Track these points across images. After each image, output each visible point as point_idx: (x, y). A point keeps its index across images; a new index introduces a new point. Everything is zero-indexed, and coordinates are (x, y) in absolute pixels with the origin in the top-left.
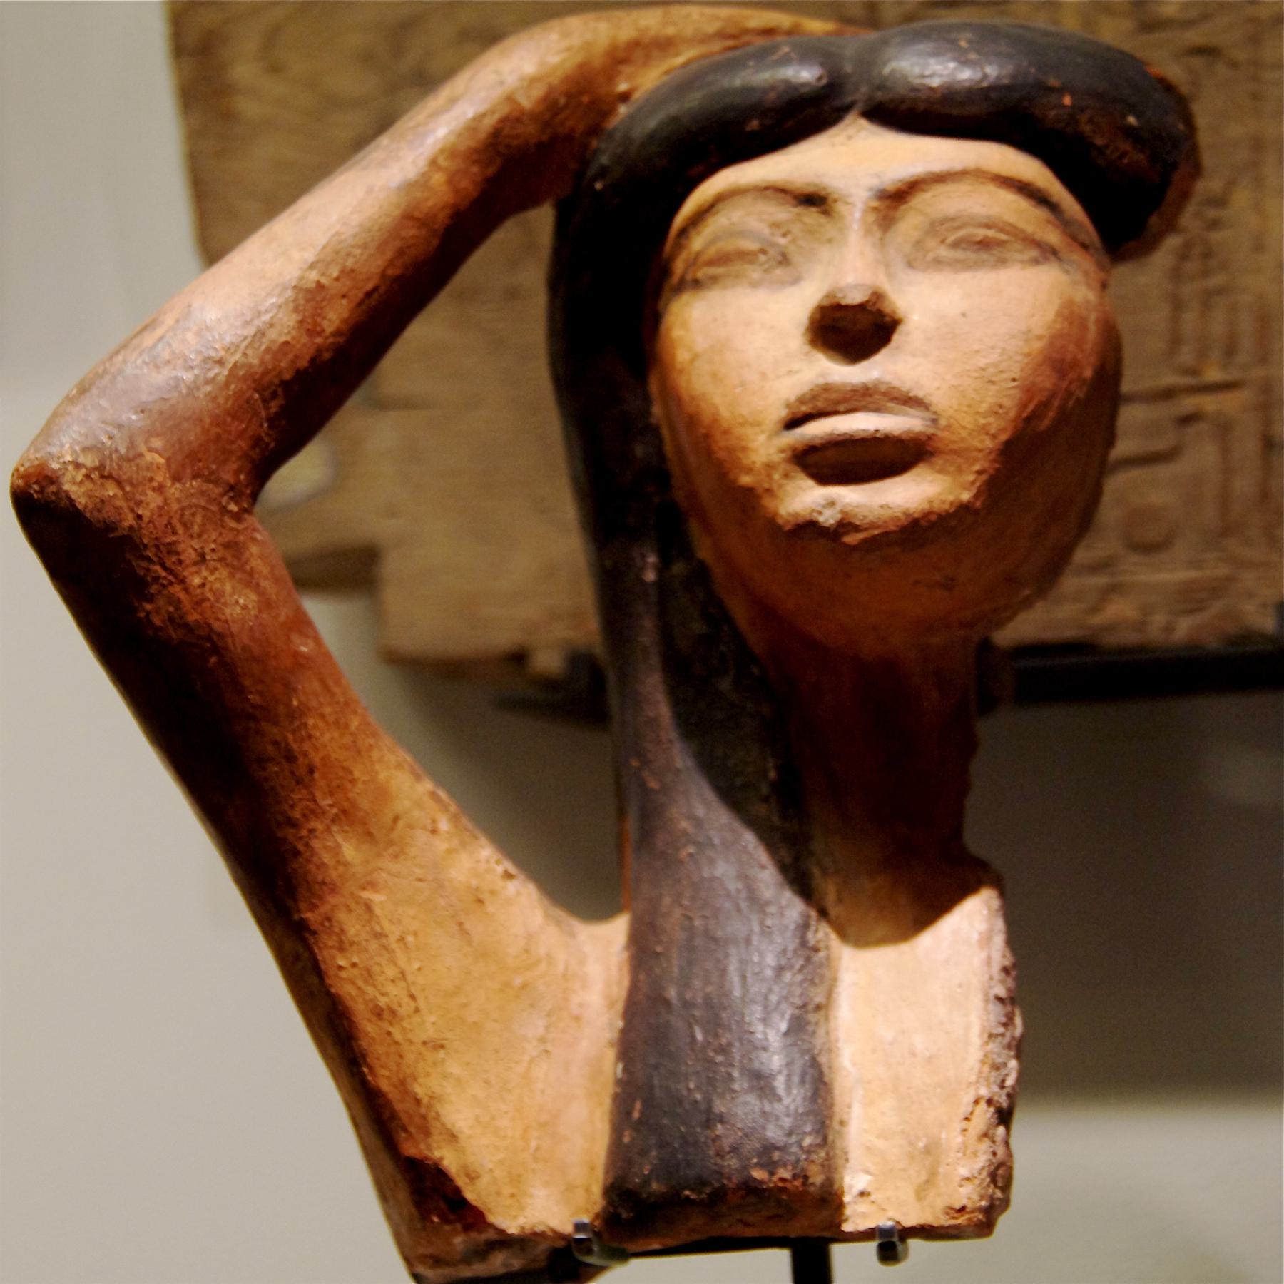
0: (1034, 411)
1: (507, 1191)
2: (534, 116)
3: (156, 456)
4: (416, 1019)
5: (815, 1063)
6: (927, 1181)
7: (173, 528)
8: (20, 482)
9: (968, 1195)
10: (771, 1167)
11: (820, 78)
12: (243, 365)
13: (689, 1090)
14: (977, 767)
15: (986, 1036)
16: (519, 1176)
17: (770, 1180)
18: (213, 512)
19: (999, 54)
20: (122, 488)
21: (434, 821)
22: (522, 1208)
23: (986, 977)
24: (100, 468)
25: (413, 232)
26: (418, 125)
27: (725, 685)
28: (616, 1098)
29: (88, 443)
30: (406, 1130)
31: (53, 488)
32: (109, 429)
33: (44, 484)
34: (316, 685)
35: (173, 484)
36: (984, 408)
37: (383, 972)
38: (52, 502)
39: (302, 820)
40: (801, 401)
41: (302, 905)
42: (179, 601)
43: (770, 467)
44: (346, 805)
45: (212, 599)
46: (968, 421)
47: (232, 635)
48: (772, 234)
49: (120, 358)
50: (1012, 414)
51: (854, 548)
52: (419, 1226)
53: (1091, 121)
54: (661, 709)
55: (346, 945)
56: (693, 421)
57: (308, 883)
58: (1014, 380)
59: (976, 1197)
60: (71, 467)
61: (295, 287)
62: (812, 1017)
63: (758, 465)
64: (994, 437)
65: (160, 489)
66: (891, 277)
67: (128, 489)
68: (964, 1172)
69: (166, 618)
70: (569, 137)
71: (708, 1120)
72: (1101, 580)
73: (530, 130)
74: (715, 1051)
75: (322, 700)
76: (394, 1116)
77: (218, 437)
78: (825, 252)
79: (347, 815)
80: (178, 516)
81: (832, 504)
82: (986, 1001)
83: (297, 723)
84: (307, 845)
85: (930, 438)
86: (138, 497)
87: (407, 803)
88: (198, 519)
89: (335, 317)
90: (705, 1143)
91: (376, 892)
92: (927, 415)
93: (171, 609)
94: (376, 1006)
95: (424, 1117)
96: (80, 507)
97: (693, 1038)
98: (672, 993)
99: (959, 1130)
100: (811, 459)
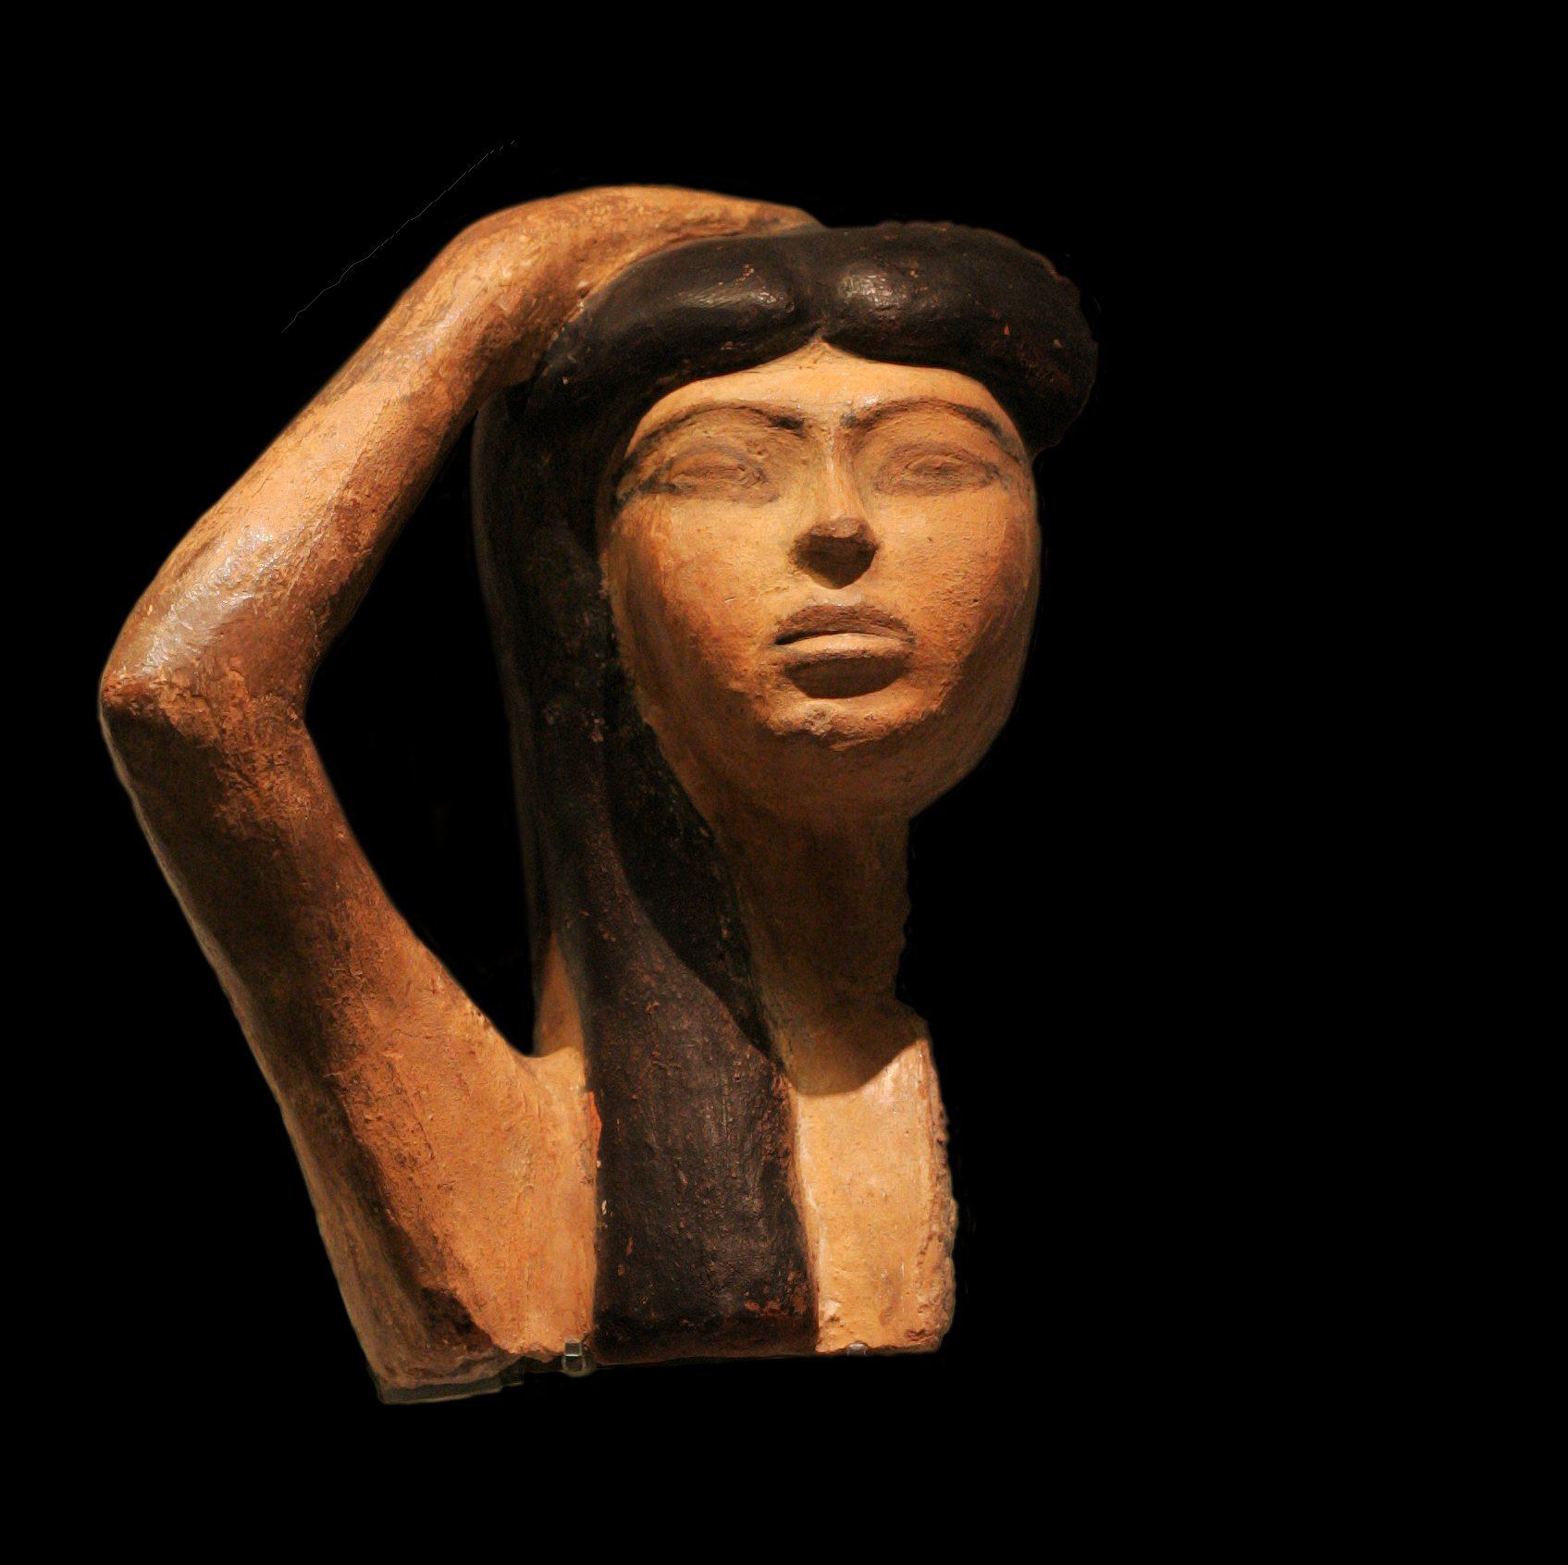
0: (990, 628)
1: (509, 1316)
2: (511, 320)
3: (237, 674)
6: (891, 1308)
7: (250, 739)
10: (761, 1301)
15: (934, 1178)
18: (281, 722)
20: (210, 706)
22: (521, 1331)
24: (191, 688)
25: (423, 442)
26: (416, 334)
28: (601, 1233)
29: (180, 664)
30: (424, 1265)
31: (151, 707)
35: (251, 700)
36: (951, 627)
37: (405, 1125)
40: (793, 619)
41: (333, 1066)
42: (251, 803)
43: (762, 677)
44: (372, 974)
45: (278, 800)
46: (937, 639)
48: (749, 451)
49: (818, 629)
50: (974, 632)
54: (614, 867)
56: (678, 626)
57: (340, 1046)
59: (932, 1322)
60: (166, 687)
61: (337, 507)
63: (749, 674)
64: (959, 653)
65: (240, 705)
68: (922, 1300)
70: (537, 333)
71: (701, 1258)
73: (509, 334)
74: (700, 1194)
76: (413, 1252)
79: (372, 984)
80: (254, 728)
81: (822, 715)
82: (932, 1146)
83: (338, 905)
84: (341, 1012)
88: (269, 730)
91: (396, 1051)
92: (906, 636)
94: (400, 1155)
96: (174, 723)
98: (652, 1139)
99: (916, 1263)
100: (803, 674)
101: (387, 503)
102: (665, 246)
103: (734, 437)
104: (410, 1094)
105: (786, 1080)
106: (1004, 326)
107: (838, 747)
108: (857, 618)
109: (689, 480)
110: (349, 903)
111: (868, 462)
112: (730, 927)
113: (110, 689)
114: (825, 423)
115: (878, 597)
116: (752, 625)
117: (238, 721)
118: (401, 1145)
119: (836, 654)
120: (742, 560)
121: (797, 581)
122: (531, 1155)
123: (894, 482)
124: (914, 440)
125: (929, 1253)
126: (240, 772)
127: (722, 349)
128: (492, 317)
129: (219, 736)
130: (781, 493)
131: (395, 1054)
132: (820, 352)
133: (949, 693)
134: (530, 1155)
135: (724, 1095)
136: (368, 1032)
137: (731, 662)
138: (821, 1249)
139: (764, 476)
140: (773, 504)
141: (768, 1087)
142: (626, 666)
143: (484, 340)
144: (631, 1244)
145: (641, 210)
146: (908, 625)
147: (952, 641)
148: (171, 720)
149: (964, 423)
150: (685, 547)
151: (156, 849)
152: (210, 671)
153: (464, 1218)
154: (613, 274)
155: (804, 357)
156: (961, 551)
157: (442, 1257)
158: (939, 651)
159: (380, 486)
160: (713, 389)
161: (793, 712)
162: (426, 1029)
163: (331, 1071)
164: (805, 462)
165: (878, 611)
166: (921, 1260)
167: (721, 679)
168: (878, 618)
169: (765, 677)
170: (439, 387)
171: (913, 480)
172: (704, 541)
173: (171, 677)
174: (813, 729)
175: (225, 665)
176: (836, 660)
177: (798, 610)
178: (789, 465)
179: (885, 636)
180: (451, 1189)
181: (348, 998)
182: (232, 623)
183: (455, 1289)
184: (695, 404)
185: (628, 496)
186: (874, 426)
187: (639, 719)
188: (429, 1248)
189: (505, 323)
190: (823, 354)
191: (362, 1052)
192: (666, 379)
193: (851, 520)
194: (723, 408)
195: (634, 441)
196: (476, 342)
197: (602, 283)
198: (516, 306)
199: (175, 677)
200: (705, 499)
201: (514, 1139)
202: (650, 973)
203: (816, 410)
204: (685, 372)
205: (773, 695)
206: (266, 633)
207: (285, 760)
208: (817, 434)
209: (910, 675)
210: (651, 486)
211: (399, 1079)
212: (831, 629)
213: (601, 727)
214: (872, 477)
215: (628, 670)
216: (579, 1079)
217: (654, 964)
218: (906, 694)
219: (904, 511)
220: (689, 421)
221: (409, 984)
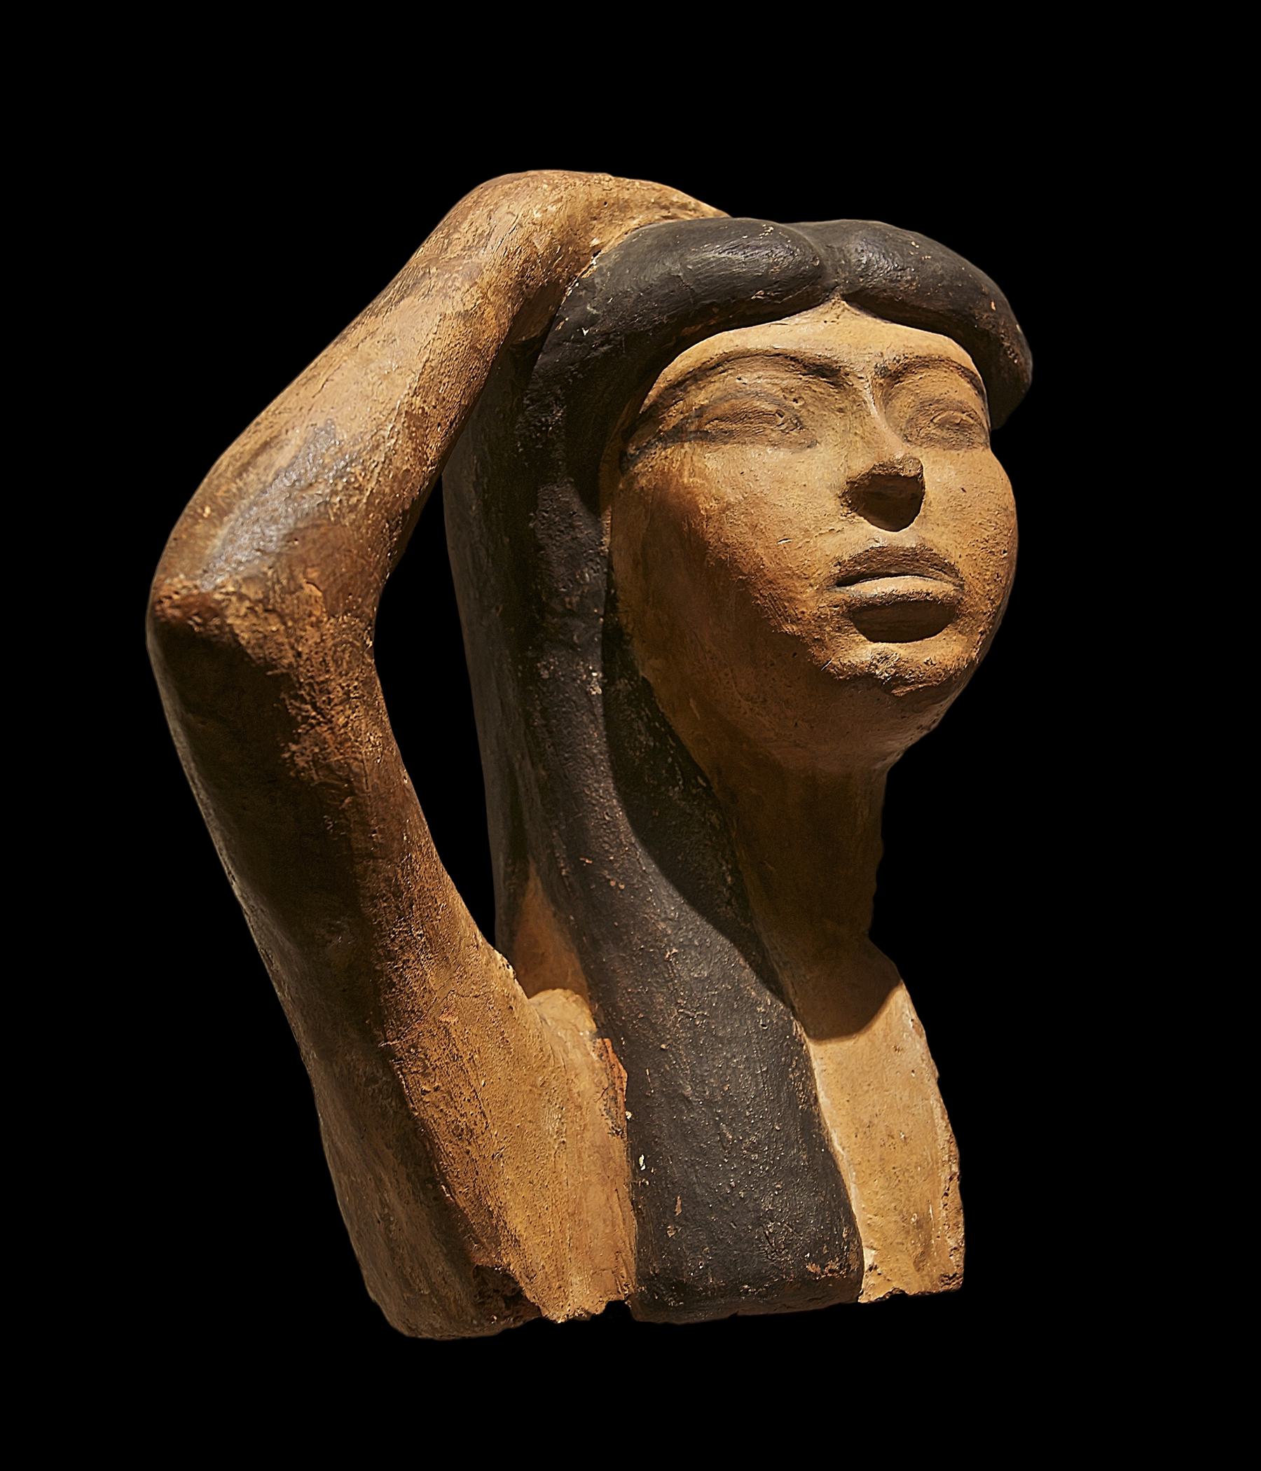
3: (314, 588)
6: (923, 1253)
7: (327, 666)
10: (821, 1261)
17: (823, 1273)
20: (285, 623)
24: (264, 601)
27: (675, 793)
31: (217, 621)
33: (207, 616)
38: (215, 636)
40: (856, 560)
43: (820, 619)
49: (881, 570)
60: (234, 599)
65: (317, 625)
67: (290, 624)
80: (331, 653)
84: (401, 976)
88: (347, 656)
93: (317, 750)
96: (243, 642)
108: (918, 560)
109: (723, 426)
112: (732, 872)
113: (164, 600)
116: (809, 566)
117: (316, 643)
126: (315, 708)
129: (293, 660)
136: (427, 995)
142: (625, 622)
144: (679, 1203)
148: (240, 638)
151: (200, 794)
152: (284, 582)
157: (496, 1232)
164: (841, 410)
167: (773, 623)
173: (240, 587)
175: (301, 576)
187: (636, 672)
191: (420, 1016)
192: (687, 331)
195: (660, 384)
199: (244, 586)
206: (344, 543)
207: (361, 692)
210: (678, 435)
211: (454, 1045)
215: (626, 626)
221: (461, 939)
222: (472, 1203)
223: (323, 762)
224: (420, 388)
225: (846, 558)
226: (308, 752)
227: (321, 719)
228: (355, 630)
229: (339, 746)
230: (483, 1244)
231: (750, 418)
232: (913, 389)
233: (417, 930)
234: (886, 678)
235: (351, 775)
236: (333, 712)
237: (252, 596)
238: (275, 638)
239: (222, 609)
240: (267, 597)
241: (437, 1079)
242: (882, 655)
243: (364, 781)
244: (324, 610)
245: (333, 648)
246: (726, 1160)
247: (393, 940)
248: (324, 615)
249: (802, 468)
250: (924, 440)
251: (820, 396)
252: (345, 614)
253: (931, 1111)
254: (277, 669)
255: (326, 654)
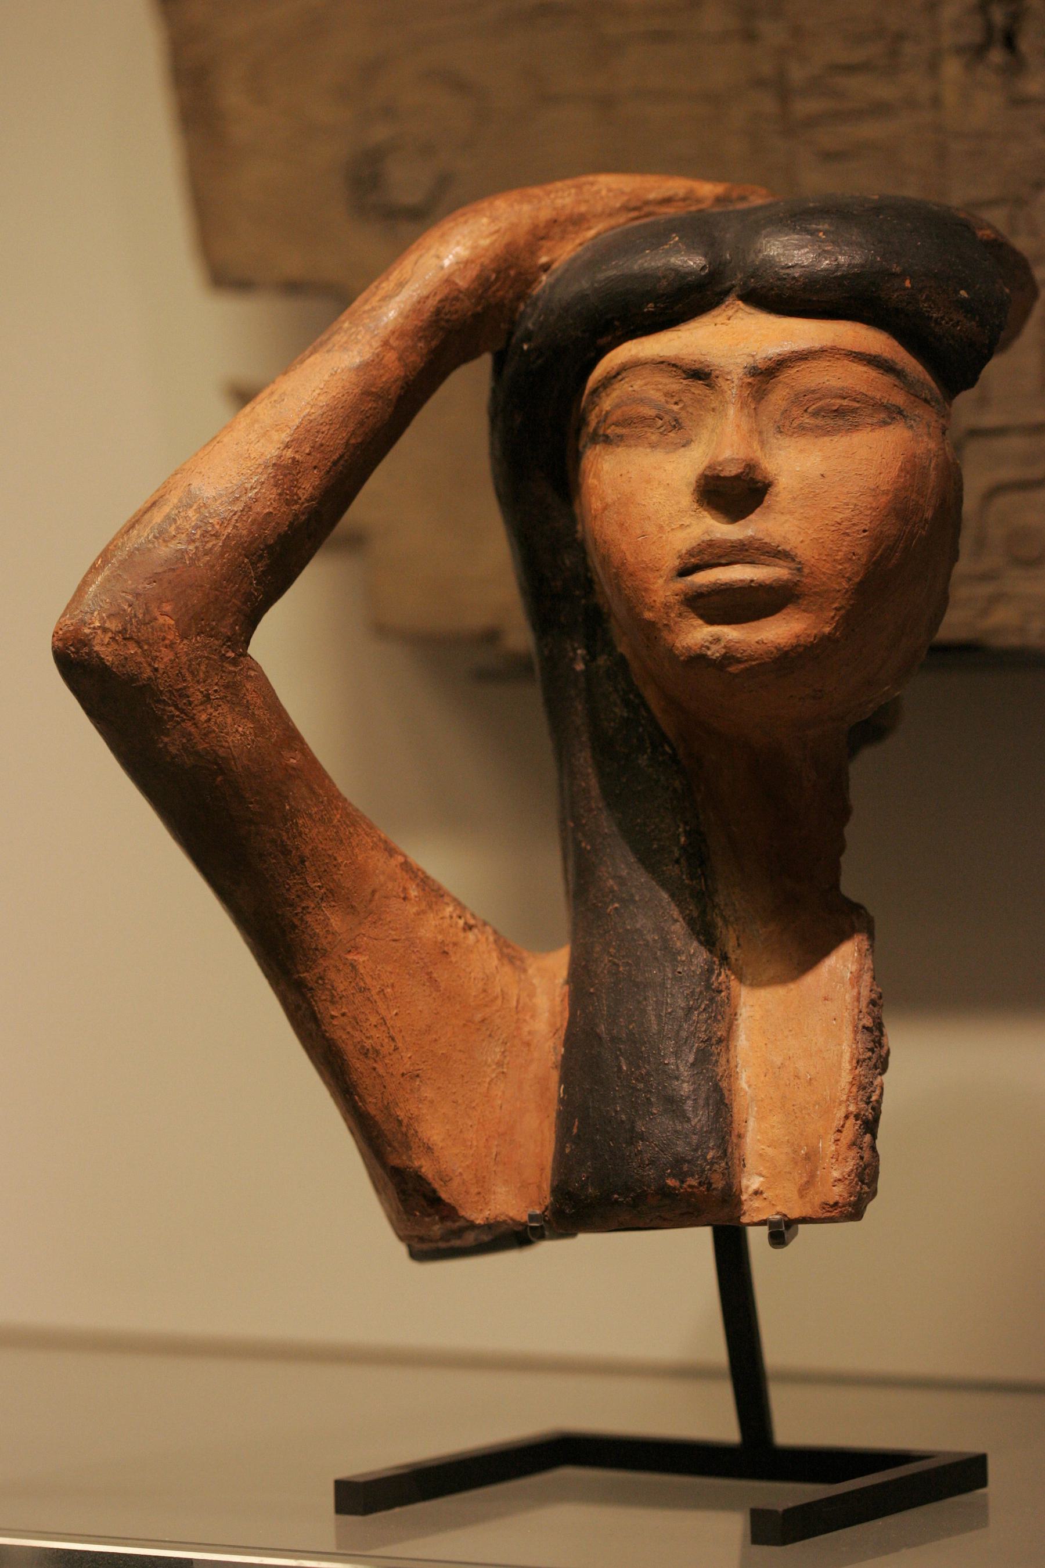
0: (881, 555)
1: (474, 1190)
2: (469, 293)
3: (167, 618)
4: (396, 1056)
5: (717, 1089)
6: (808, 1182)
7: (183, 676)
8: (60, 644)
9: (837, 1193)
10: (682, 1177)
11: (703, 268)
12: (235, 536)
13: (616, 1112)
14: (850, 831)
15: (855, 1061)
16: (484, 1177)
17: (681, 1187)
19: (849, 244)
20: (141, 647)
21: (405, 889)
23: (856, 1011)
26: (373, 309)
27: (643, 760)
28: (559, 1113)
29: (113, 610)
31: (86, 650)
32: (129, 597)
34: (304, 790)
37: (367, 1019)
38: (86, 660)
39: (297, 900)
40: (690, 553)
41: (300, 968)
42: (190, 734)
43: (667, 606)
47: (234, 758)
48: (667, 402)
50: (864, 560)
51: (736, 675)
52: (405, 1217)
53: (928, 299)
55: (337, 999)
58: (864, 531)
59: (846, 1195)
60: (99, 632)
62: (714, 1049)
65: (171, 646)
66: (763, 443)
67: (146, 647)
68: (836, 1174)
69: (181, 747)
72: (986, 589)
74: (637, 1080)
75: (309, 802)
77: (217, 598)
78: (710, 420)
79: (332, 894)
80: (186, 666)
82: (856, 1032)
84: (302, 919)
85: (796, 584)
86: (155, 654)
87: (382, 878)
88: (203, 668)
89: (308, 486)
90: (629, 1156)
92: (793, 565)
93: (184, 741)
94: (363, 1047)
95: (405, 1135)
96: (108, 664)
97: (620, 1068)
98: (602, 1028)
99: (833, 1140)
101: (332, 460)
102: (624, 224)
103: (653, 389)
104: (374, 992)
105: (729, 973)
106: (906, 279)
107: (733, 669)
108: (747, 550)
109: (619, 431)
110: (300, 822)
111: (771, 408)
114: (729, 373)
115: (767, 530)
116: (660, 559)
118: (363, 1038)
119: (726, 584)
120: (654, 500)
121: (698, 518)
122: (506, 1043)
123: (794, 425)
124: (813, 386)
125: (845, 1131)
126: (177, 708)
127: (646, 310)
128: (446, 291)
130: (694, 438)
131: (358, 956)
132: (733, 311)
133: (842, 617)
134: (504, 1043)
135: (667, 988)
137: (644, 594)
138: (750, 1128)
139: (679, 424)
140: (686, 448)
141: (708, 980)
143: (438, 312)
144: (577, 1123)
145: (604, 192)
146: (796, 556)
147: (841, 570)
149: (865, 369)
150: (610, 491)
152: (141, 616)
153: (432, 1102)
154: (574, 250)
155: (719, 315)
156: (852, 486)
158: (829, 579)
159: (322, 445)
160: (640, 348)
161: (693, 638)
162: (393, 933)
163: (298, 972)
164: (713, 410)
165: (766, 543)
166: (838, 1137)
167: (637, 610)
168: (767, 549)
169: (669, 607)
170: (390, 354)
171: (812, 422)
172: (624, 485)
173: (105, 622)
174: (709, 653)
176: (727, 589)
177: (695, 544)
178: (702, 413)
179: (774, 566)
180: (418, 1076)
181: (308, 907)
182: (165, 572)
183: (421, 1167)
184: (623, 361)
185: (585, 447)
186: (777, 374)
188: (394, 1130)
189: (461, 296)
190: (737, 311)
192: (602, 341)
193: (738, 459)
194: (646, 363)
195: (584, 398)
196: (429, 314)
197: (562, 258)
198: (473, 281)
199: (108, 622)
200: (630, 446)
201: (487, 1029)
202: (614, 877)
203: (722, 362)
204: (619, 333)
205: (676, 623)
208: (723, 384)
209: (800, 601)
212: (723, 561)
213: (583, 658)
214: (775, 422)
216: (563, 973)
217: (335, 877)
218: (797, 619)
219: (801, 451)
220: (620, 377)
221: (374, 892)
222: (382, 1111)
223: (192, 750)
224: (292, 441)
225: (684, 551)
226: (178, 743)
227: (185, 717)
228: (210, 647)
229: (203, 737)
230: (394, 1148)
231: (635, 423)
232: (788, 382)
233: (314, 882)
234: (717, 657)
235: (218, 759)
236: (195, 712)
237: (113, 629)
238: (134, 659)
239: (90, 640)
240: (125, 629)
241: (344, 1006)
242: (714, 637)
243: (233, 763)
244: (177, 634)
245: (188, 663)
246: (617, 1088)
247: (288, 890)
248: (177, 638)
249: (669, 467)
250: (796, 430)
251: (699, 397)
252: (198, 634)
253: (841, 1055)
254: (139, 681)
255: (181, 668)
